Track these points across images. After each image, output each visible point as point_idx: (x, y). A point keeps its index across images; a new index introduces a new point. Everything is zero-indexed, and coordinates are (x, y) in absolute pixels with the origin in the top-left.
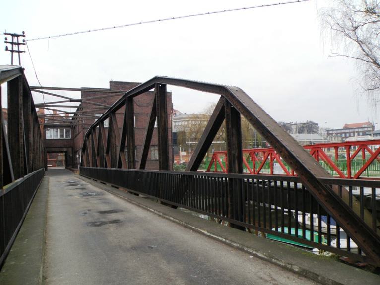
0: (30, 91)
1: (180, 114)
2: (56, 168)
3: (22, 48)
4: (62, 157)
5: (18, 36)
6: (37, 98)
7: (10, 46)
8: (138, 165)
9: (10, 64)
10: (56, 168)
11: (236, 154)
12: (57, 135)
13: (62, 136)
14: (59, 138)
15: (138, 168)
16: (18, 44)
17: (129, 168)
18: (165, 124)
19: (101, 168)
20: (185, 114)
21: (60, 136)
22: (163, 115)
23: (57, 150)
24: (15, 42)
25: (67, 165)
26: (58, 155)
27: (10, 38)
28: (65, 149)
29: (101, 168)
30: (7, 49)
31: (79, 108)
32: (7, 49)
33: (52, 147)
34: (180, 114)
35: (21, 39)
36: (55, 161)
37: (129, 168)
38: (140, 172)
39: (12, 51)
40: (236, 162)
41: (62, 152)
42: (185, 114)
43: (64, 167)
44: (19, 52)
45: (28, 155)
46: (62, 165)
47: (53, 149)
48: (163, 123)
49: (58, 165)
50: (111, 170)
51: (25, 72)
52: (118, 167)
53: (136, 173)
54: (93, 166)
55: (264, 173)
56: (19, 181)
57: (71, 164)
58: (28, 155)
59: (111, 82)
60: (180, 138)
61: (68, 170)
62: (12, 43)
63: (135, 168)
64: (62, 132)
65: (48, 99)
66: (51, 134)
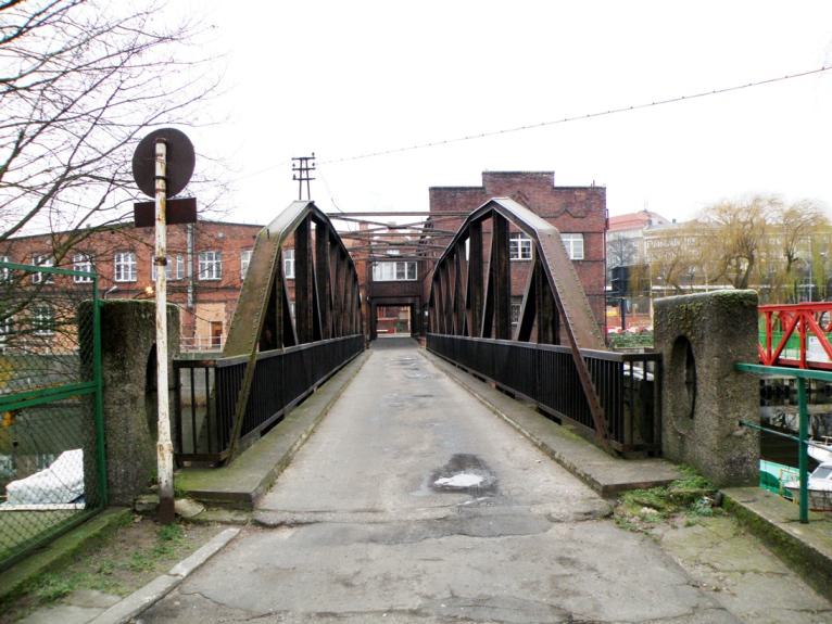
0: (328, 220)
1: (660, 223)
2: (396, 335)
3: (312, 174)
4: (405, 315)
5: (306, 159)
6: (339, 226)
7: (297, 174)
8: (516, 333)
9: (297, 199)
10: (396, 335)
11: (551, 319)
12: (392, 274)
13: (400, 274)
14: (395, 279)
15: (514, 340)
16: (307, 169)
17: (539, 342)
18: (506, 270)
19: (459, 337)
20: (674, 221)
21: (409, 273)
22: (504, 257)
23: (394, 301)
24: (304, 169)
25: (413, 331)
26: (399, 311)
27: (298, 163)
28: (410, 301)
29: (459, 337)
30: (294, 179)
31: (428, 225)
32: (294, 179)
33: (384, 297)
34: (660, 223)
35: (310, 162)
36: (395, 322)
37: (539, 342)
38: (519, 348)
39: (301, 180)
40: (550, 329)
41: (407, 305)
42: (674, 221)
43: (409, 335)
44: (308, 179)
45: (324, 314)
46: (405, 330)
47: (388, 301)
48: (503, 270)
49: (399, 331)
50: (472, 342)
51: (316, 204)
52: (484, 336)
53: (512, 348)
54: (442, 332)
55: (788, 358)
56: (304, 346)
57: (419, 329)
58: (324, 314)
59: (484, 174)
60: (634, 278)
61: (413, 340)
62: (301, 170)
63: (556, 341)
64: (400, 266)
65: (354, 227)
66: (385, 273)
